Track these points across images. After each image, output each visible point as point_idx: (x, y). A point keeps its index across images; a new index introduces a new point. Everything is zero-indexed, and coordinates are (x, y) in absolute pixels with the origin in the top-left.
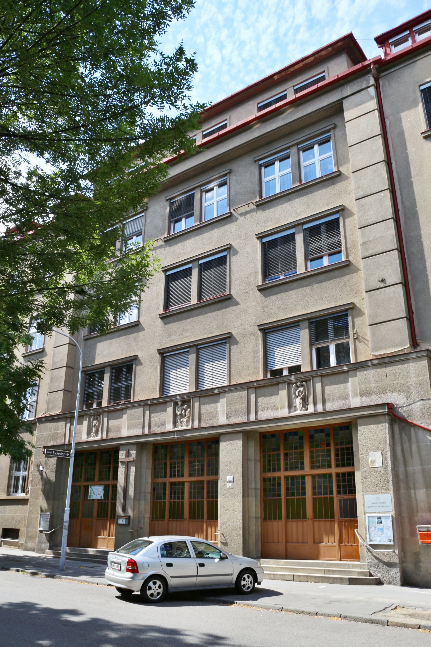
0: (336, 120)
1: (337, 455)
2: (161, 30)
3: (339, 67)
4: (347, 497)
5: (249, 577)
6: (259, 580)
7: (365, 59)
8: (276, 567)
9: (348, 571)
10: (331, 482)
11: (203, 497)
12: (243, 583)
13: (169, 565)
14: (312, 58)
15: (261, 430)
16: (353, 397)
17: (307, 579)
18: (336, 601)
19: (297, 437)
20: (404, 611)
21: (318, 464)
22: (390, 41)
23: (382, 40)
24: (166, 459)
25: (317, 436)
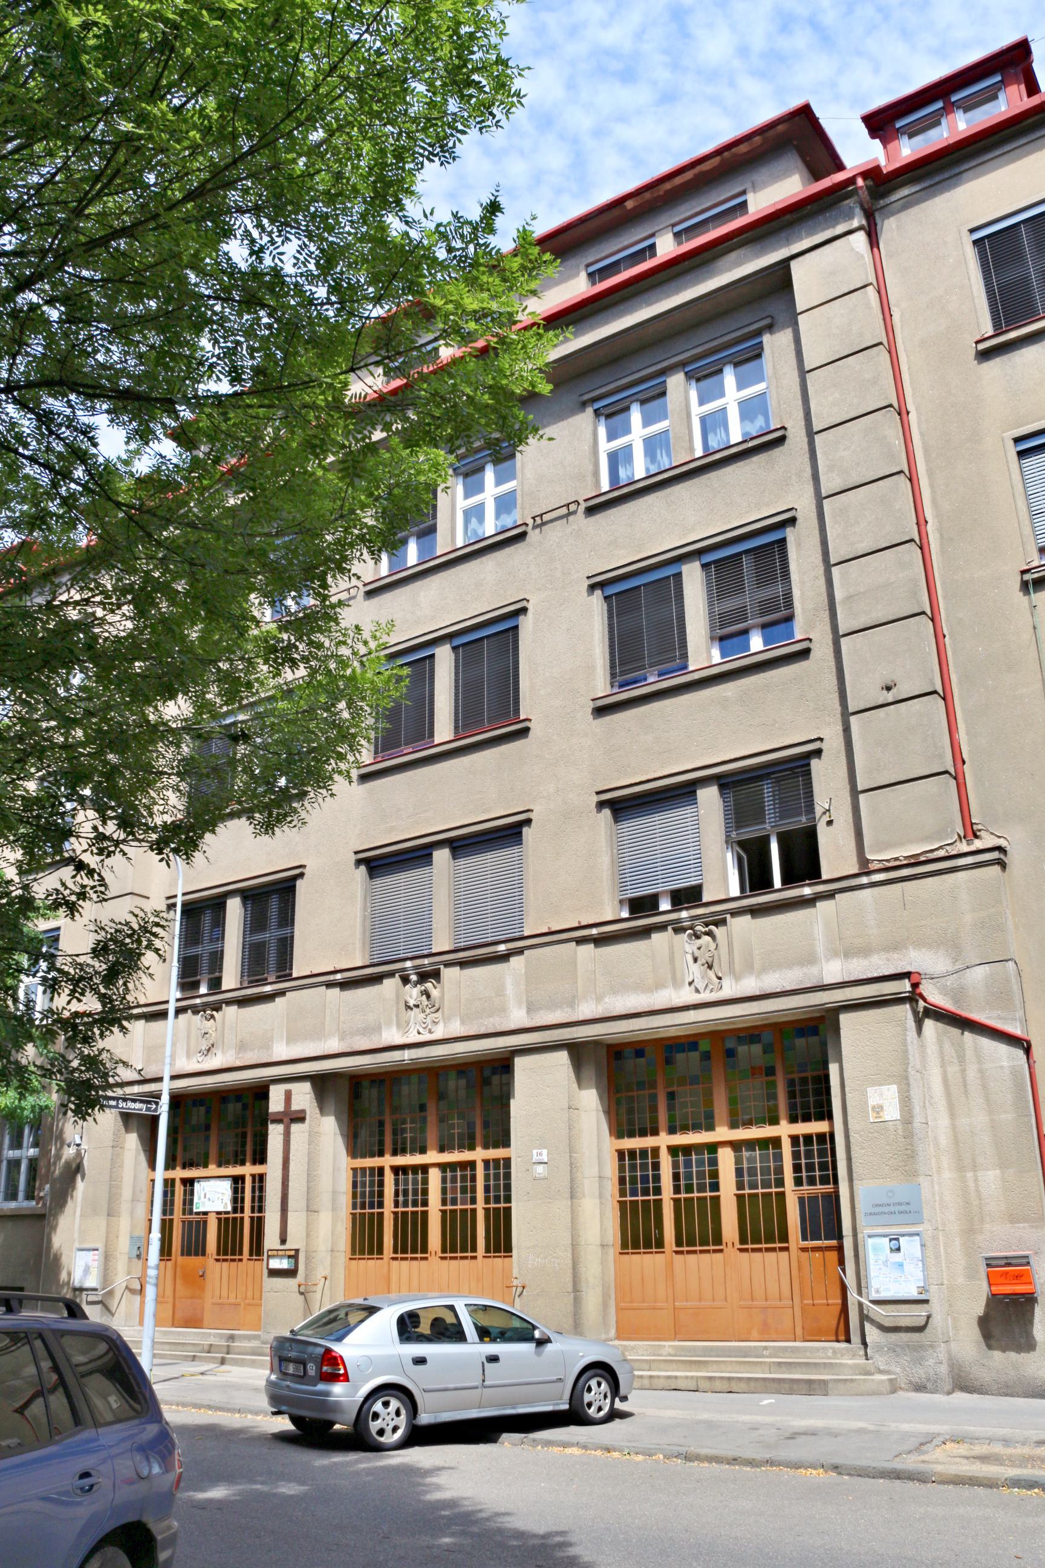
0: (774, 307)
1: (791, 1095)
2: (447, 155)
3: (780, 188)
4: (820, 1189)
5: (599, 1384)
6: (622, 1392)
7: (840, 167)
8: (654, 1361)
9: (825, 1364)
10: (779, 1157)
11: (473, 1201)
12: (587, 1397)
13: (420, 1361)
14: (716, 161)
15: (610, 1042)
16: (828, 960)
17: (730, 1387)
18: (805, 1434)
19: (695, 1056)
20: (962, 1449)
21: (747, 1117)
22: (898, 125)
23: (881, 123)
24: (381, 1113)
25: (742, 1050)
